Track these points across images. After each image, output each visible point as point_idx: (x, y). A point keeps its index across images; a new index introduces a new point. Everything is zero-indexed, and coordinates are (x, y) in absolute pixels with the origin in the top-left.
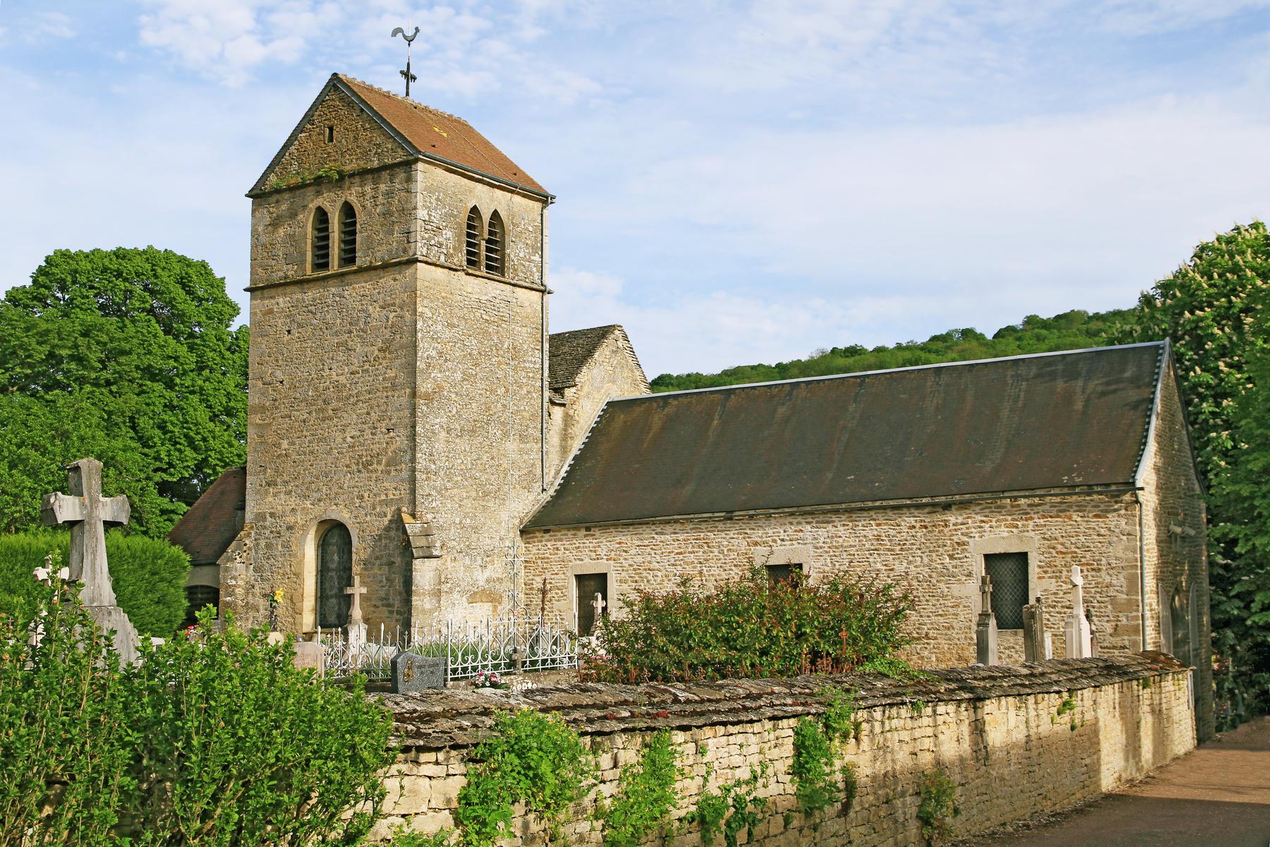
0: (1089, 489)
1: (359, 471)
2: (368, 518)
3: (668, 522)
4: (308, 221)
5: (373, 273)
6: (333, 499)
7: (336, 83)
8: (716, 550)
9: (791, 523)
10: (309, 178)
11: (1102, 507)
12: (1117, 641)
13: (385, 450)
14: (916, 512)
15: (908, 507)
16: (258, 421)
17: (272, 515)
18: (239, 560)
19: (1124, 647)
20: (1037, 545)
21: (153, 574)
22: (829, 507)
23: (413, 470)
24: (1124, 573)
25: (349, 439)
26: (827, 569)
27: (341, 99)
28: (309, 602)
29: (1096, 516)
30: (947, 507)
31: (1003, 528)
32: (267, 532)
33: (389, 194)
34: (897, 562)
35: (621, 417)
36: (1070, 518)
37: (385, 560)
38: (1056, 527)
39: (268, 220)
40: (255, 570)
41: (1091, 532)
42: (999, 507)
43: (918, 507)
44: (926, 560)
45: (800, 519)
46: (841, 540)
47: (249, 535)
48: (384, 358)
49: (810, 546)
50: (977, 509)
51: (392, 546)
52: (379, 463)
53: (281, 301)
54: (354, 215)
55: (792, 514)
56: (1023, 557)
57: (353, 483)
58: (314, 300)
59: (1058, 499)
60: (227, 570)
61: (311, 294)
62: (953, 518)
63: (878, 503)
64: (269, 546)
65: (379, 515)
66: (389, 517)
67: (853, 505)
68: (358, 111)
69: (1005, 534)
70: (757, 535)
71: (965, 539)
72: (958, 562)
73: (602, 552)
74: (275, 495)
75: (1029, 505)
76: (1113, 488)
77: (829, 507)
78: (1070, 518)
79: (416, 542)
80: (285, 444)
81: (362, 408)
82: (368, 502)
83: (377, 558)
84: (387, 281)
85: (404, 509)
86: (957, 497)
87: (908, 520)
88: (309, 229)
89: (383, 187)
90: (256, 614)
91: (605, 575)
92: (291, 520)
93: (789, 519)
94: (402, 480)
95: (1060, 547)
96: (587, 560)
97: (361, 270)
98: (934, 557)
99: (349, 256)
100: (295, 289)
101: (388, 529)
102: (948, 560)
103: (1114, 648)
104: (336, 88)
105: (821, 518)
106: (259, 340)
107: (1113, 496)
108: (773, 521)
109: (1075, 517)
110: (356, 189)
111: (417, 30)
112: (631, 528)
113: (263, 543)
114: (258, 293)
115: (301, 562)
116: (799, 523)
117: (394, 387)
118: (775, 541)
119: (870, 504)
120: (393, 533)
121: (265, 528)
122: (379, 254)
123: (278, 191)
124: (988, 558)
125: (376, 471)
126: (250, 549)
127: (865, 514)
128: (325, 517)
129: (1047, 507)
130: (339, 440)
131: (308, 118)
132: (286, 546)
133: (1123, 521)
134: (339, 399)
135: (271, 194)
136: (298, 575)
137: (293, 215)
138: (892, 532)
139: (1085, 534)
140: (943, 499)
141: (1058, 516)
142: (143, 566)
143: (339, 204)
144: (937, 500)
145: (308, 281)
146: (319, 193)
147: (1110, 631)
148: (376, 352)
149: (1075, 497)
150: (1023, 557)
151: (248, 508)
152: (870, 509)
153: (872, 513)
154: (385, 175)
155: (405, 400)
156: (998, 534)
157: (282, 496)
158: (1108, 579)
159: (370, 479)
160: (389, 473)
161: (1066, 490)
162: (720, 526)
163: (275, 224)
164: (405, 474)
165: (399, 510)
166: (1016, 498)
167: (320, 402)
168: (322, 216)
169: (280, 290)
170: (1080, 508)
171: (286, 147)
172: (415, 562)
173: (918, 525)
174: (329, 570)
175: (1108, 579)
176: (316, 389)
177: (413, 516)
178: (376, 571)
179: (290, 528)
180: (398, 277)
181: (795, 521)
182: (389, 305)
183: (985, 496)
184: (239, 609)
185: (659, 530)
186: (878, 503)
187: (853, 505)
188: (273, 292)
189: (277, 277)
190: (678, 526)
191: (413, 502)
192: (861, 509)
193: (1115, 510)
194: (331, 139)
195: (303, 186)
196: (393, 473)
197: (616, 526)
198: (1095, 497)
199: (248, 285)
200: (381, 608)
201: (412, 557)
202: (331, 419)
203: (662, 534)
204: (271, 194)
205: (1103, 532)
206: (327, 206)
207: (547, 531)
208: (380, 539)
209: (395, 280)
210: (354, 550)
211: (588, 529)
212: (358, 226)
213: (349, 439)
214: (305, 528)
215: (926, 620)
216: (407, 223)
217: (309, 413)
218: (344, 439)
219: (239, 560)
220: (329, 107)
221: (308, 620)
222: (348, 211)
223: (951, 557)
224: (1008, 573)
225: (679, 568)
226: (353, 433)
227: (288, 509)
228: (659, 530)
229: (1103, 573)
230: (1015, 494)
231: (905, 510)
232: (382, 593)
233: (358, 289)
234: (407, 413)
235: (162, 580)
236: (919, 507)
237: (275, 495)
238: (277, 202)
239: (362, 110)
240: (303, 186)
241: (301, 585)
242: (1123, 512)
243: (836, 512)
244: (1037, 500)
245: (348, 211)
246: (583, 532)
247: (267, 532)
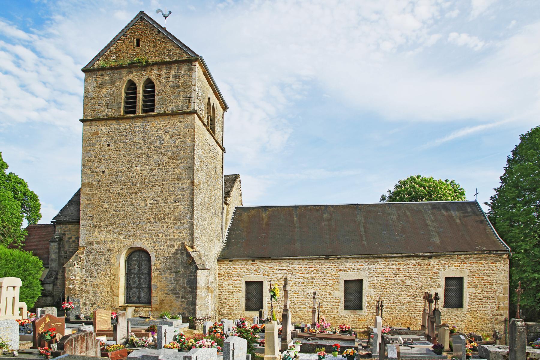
0: (490, 252)
1: (156, 222)
2: (162, 247)
3: (296, 259)
4: (122, 87)
5: (166, 117)
6: (139, 236)
7: (142, 17)
8: (320, 273)
9: (358, 262)
10: (126, 62)
11: (495, 260)
12: (499, 312)
13: (173, 212)
14: (416, 259)
15: (413, 257)
16: (87, 192)
17: (97, 243)
18: (77, 266)
19: (502, 315)
20: (468, 274)
21: (25, 271)
22: (376, 256)
23: (192, 224)
24: (503, 286)
25: (149, 205)
26: (374, 282)
27: (145, 25)
28: (122, 291)
29: (492, 263)
30: (430, 257)
31: (454, 267)
32: (94, 252)
33: (177, 77)
34: (407, 280)
35: (245, 215)
36: (481, 264)
37: (173, 270)
38: (475, 267)
39: (95, 84)
40: (86, 271)
41: (490, 269)
42: (452, 258)
43: (417, 257)
44: (420, 279)
45: (362, 260)
46: (381, 270)
47: (82, 253)
48: (173, 163)
49: (367, 272)
50: (443, 258)
51: (177, 263)
52: (169, 218)
53: (104, 128)
54: (154, 87)
55: (358, 258)
56: (461, 279)
57: (151, 228)
58: (126, 129)
59: (477, 256)
60: (69, 271)
61: (124, 125)
62: (433, 262)
63: (399, 255)
64: (95, 259)
65: (169, 246)
66: (176, 247)
67: (388, 255)
68: (157, 32)
69: (455, 269)
70: (341, 266)
71: (437, 271)
72: (434, 280)
73: (261, 271)
74: (99, 232)
75: (465, 258)
76: (499, 252)
77: (376, 256)
78: (481, 264)
79: (198, 261)
80: (106, 205)
81: (158, 189)
82: (162, 238)
83: (168, 269)
84: (175, 121)
85: (186, 244)
86: (435, 253)
87: (412, 262)
88: (123, 92)
89: (172, 72)
90: (88, 295)
91: (262, 282)
92: (110, 246)
93: (357, 260)
94: (185, 229)
95: (477, 275)
96: (252, 275)
97: (159, 115)
98: (424, 278)
99: (149, 107)
100: (114, 123)
101: (175, 254)
102: (429, 280)
103: (498, 315)
104: (142, 19)
105: (372, 260)
106: (89, 148)
107: (499, 256)
108: (349, 260)
109: (483, 263)
110: (155, 72)
111: (170, 12)
112: (276, 261)
113: (91, 257)
114: (89, 123)
115: (118, 268)
116: (361, 262)
117: (179, 179)
118: (349, 269)
119: (396, 255)
120: (178, 256)
121: (93, 249)
122: (170, 107)
123: (103, 69)
124: (447, 279)
125: (168, 222)
126: (83, 260)
127: (393, 259)
128: (133, 246)
129: (472, 259)
130: (142, 205)
131: (124, 33)
132: (108, 260)
133: (503, 265)
134: (142, 183)
135: (98, 70)
136: (116, 276)
137: (113, 82)
138: (405, 267)
139: (487, 270)
140: (429, 254)
141: (477, 263)
142: (19, 266)
143: (144, 79)
144: (426, 254)
145: (122, 119)
146: (130, 72)
147: (496, 308)
148: (167, 159)
149: (484, 255)
150: (461, 279)
151: (81, 239)
152: (396, 257)
153: (396, 259)
154: (175, 66)
155: (186, 186)
156: (449, 268)
157: (104, 233)
158: (496, 288)
159: (163, 227)
160: (176, 224)
161: (480, 252)
162: (323, 262)
163: (101, 86)
164: (187, 225)
165: (183, 244)
166: (460, 255)
167: (130, 184)
168: (132, 86)
169: (103, 122)
170: (486, 260)
171: (108, 46)
172: (198, 272)
173: (417, 265)
174: (132, 273)
175: (496, 288)
176: (127, 177)
177: (192, 247)
178: (167, 275)
179: (109, 250)
180: (182, 120)
181: (360, 261)
182: (176, 135)
183: (447, 253)
184: (77, 292)
185: (291, 263)
186: (399, 255)
187: (388, 255)
188: (98, 123)
189: (101, 115)
190: (301, 261)
191: (192, 240)
192: (392, 257)
193: (500, 261)
194: (138, 45)
195: (121, 67)
196: (178, 224)
197: (268, 260)
198: (492, 255)
199: (82, 118)
200: (171, 295)
201: (197, 268)
202: (137, 193)
203: (292, 264)
204: (98, 70)
205: (494, 269)
206: (136, 80)
207: (230, 261)
208: (170, 259)
209: (180, 122)
210: (152, 263)
211: (253, 261)
212: (156, 92)
213: (149, 205)
214: (119, 251)
215: (419, 304)
216: (189, 92)
217: (123, 189)
218: (146, 205)
219: (77, 266)
220: (137, 28)
221: (121, 300)
222: (149, 84)
223: (431, 278)
224: (455, 285)
225: (301, 280)
226: (152, 202)
227: (108, 240)
228: (291, 263)
229: (494, 286)
230: (459, 253)
231: (411, 258)
232: (172, 287)
233: (154, 125)
234: (188, 193)
235: (30, 274)
236: (418, 257)
237: (99, 232)
238: (102, 75)
239: (159, 32)
240: (121, 67)
241: (118, 281)
242: (502, 262)
243: (380, 258)
244: (468, 256)
245: (149, 84)
246: (251, 262)
247: (94, 252)
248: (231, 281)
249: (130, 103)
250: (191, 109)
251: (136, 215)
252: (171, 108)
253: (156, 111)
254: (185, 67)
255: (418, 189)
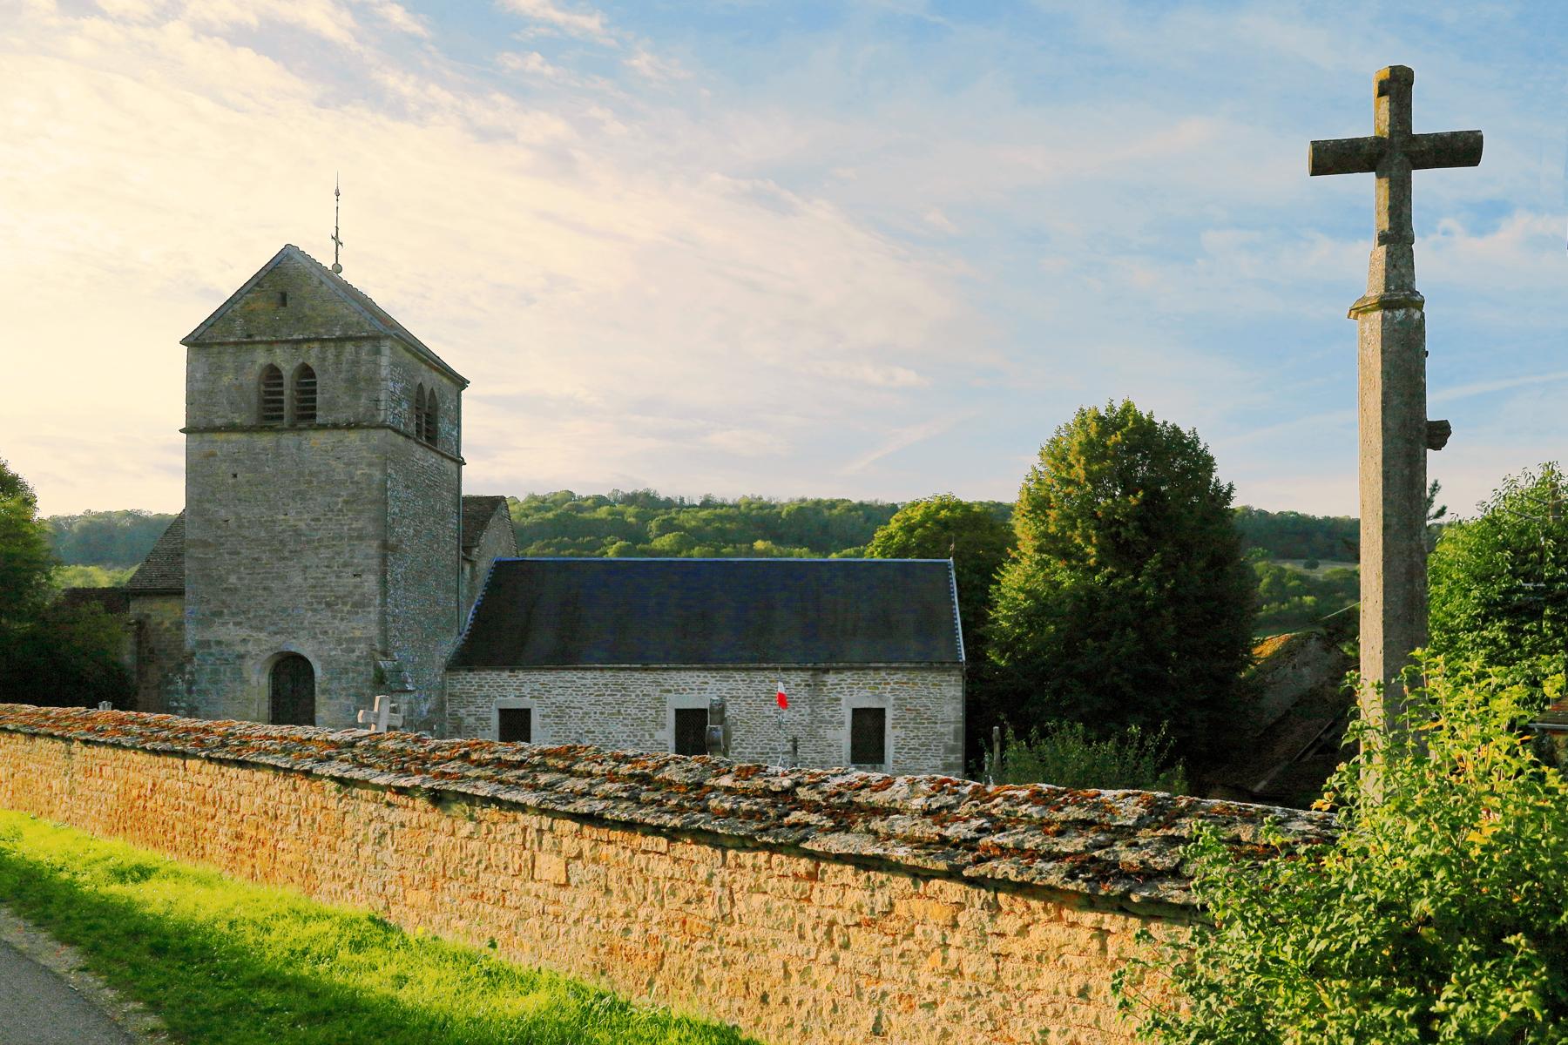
6: (291, 633)
15: (796, 669)
17: (219, 643)
30: (826, 671)
33: (356, 363)
51: (360, 679)
92: (241, 649)
117: (360, 538)
189: (218, 422)
190: (598, 673)
199: (1086, 408)
248: (472, 708)
249: (306, 400)
250: (381, 419)
251: (287, 596)
252: (342, 416)
253: (319, 420)
254: (366, 347)
255: (1123, 586)
